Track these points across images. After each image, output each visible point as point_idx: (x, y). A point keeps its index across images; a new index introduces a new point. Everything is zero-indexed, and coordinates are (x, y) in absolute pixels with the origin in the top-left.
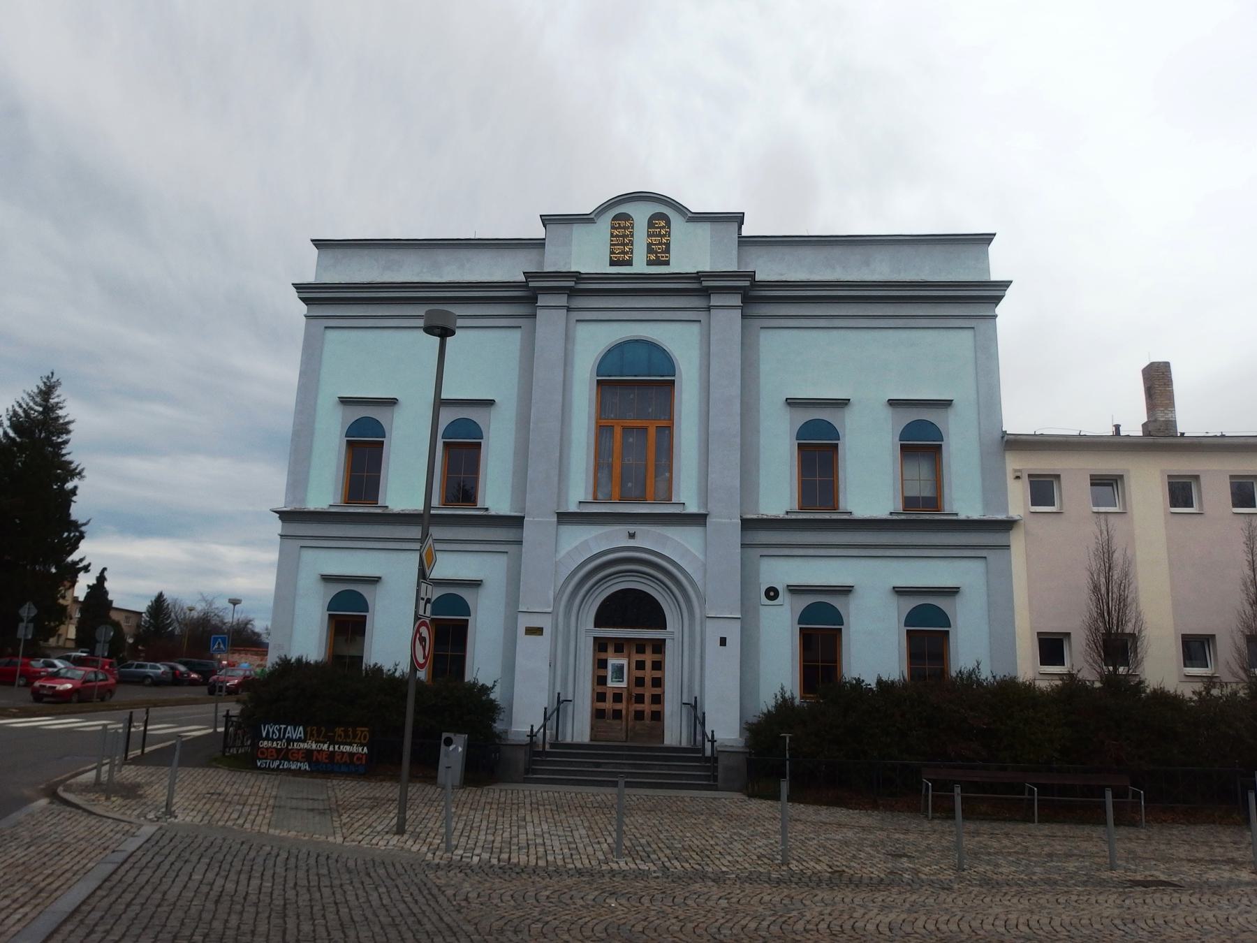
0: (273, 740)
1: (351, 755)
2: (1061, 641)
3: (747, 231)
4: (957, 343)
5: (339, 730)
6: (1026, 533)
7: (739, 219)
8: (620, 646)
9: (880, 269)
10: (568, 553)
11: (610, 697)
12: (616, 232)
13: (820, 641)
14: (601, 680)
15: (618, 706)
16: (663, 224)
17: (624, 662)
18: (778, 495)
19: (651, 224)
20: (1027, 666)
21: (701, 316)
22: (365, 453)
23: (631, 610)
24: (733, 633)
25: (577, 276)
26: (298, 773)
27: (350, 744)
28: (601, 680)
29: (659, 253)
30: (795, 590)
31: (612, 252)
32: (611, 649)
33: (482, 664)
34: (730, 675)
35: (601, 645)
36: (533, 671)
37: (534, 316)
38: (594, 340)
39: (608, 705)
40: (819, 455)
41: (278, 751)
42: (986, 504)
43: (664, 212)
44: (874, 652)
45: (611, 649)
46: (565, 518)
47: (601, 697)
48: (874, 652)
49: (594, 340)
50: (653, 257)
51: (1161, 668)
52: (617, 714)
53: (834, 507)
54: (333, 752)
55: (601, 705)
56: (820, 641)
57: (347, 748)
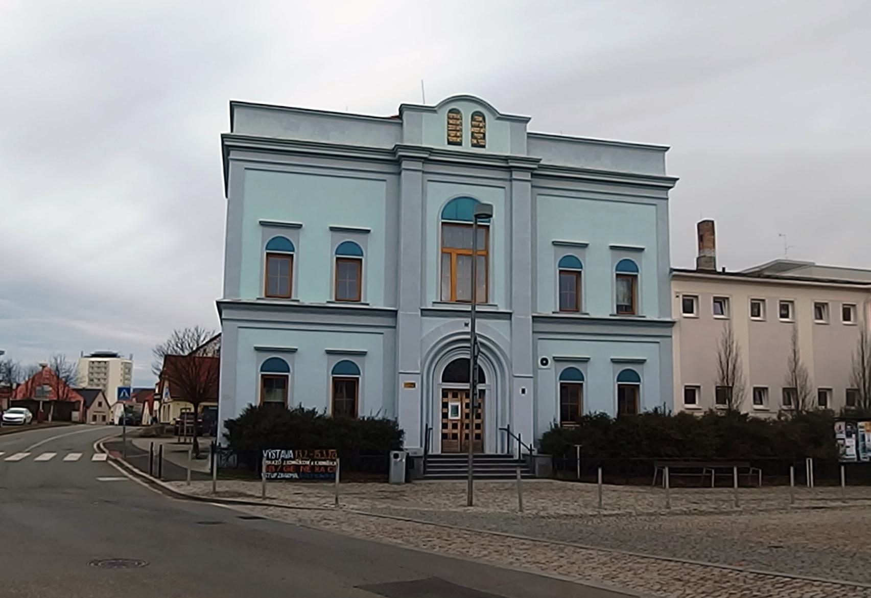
0: (272, 460)
1: (326, 467)
2: (694, 391)
3: (531, 128)
4: (647, 212)
5: (317, 452)
6: (681, 330)
7: (527, 120)
8: (455, 393)
9: (304, 133)
10: (427, 336)
11: (450, 426)
12: (451, 122)
13: (571, 392)
14: (445, 416)
15: (455, 431)
16: (481, 119)
17: (459, 404)
18: (549, 305)
19: (473, 119)
20: (678, 405)
21: (506, 184)
22: (280, 257)
23: (463, 372)
24: (529, 386)
25: (430, 150)
26: (291, 480)
27: (325, 460)
28: (445, 416)
29: (479, 140)
30: (557, 360)
31: (449, 135)
32: (450, 396)
33: (370, 405)
34: (523, 411)
35: (445, 393)
36: (415, 411)
37: (400, 174)
38: (440, 194)
39: (449, 430)
40: (571, 277)
41: (276, 467)
42: (661, 313)
43: (482, 111)
44: (600, 399)
45: (450, 396)
46: (425, 312)
47: (445, 426)
48: (600, 399)
49: (440, 194)
50: (475, 141)
51: (747, 407)
52: (455, 436)
53: (577, 310)
54: (314, 466)
55: (445, 431)
56: (571, 392)
57: (324, 463)
